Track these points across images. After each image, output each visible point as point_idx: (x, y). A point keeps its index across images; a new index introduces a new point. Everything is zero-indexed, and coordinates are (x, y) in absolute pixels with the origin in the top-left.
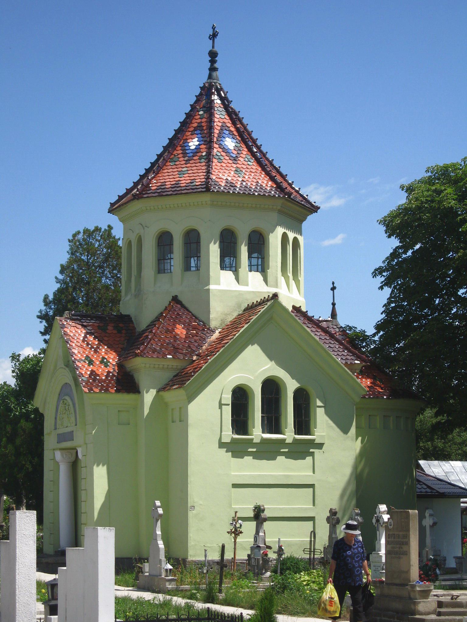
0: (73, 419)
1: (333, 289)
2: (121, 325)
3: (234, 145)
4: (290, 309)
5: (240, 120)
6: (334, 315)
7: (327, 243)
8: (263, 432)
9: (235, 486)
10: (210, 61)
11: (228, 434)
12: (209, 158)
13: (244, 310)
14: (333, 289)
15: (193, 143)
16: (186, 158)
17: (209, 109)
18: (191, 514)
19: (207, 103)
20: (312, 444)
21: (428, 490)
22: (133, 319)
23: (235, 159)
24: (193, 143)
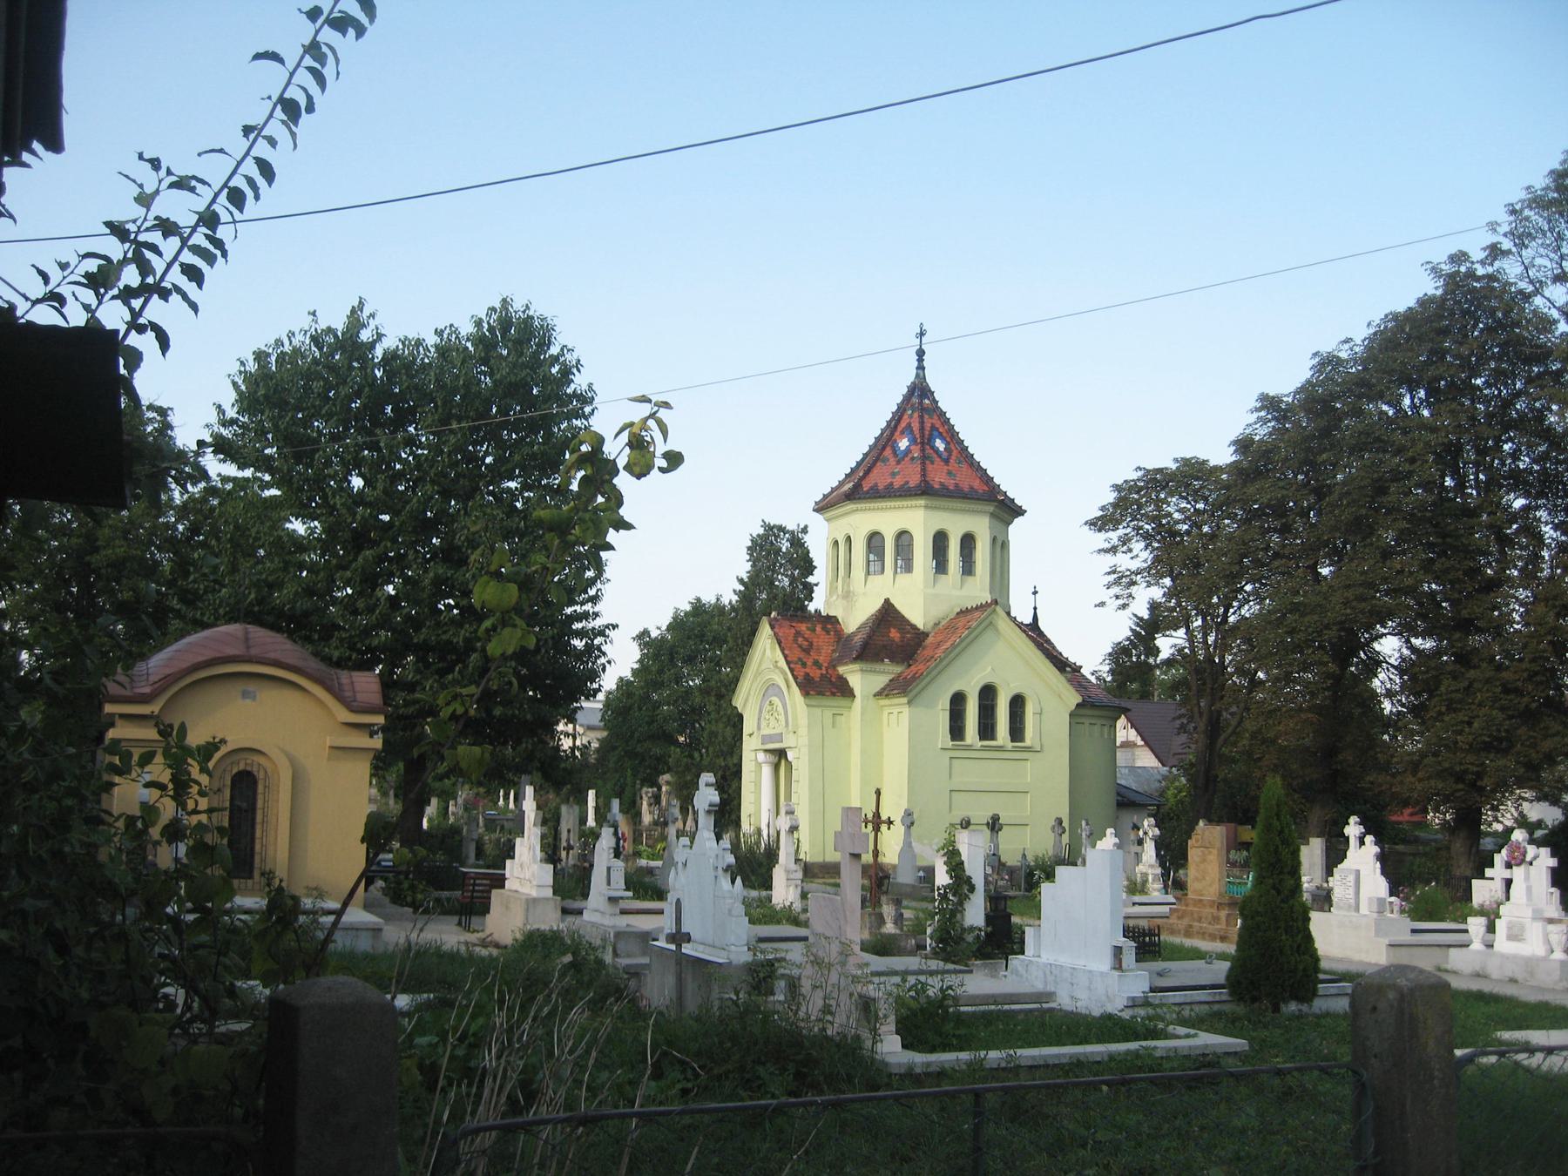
0: (782, 718)
1: (1035, 593)
2: (829, 626)
10: (918, 360)
14: (1035, 593)
22: (840, 620)
23: (947, 461)
24: (903, 444)
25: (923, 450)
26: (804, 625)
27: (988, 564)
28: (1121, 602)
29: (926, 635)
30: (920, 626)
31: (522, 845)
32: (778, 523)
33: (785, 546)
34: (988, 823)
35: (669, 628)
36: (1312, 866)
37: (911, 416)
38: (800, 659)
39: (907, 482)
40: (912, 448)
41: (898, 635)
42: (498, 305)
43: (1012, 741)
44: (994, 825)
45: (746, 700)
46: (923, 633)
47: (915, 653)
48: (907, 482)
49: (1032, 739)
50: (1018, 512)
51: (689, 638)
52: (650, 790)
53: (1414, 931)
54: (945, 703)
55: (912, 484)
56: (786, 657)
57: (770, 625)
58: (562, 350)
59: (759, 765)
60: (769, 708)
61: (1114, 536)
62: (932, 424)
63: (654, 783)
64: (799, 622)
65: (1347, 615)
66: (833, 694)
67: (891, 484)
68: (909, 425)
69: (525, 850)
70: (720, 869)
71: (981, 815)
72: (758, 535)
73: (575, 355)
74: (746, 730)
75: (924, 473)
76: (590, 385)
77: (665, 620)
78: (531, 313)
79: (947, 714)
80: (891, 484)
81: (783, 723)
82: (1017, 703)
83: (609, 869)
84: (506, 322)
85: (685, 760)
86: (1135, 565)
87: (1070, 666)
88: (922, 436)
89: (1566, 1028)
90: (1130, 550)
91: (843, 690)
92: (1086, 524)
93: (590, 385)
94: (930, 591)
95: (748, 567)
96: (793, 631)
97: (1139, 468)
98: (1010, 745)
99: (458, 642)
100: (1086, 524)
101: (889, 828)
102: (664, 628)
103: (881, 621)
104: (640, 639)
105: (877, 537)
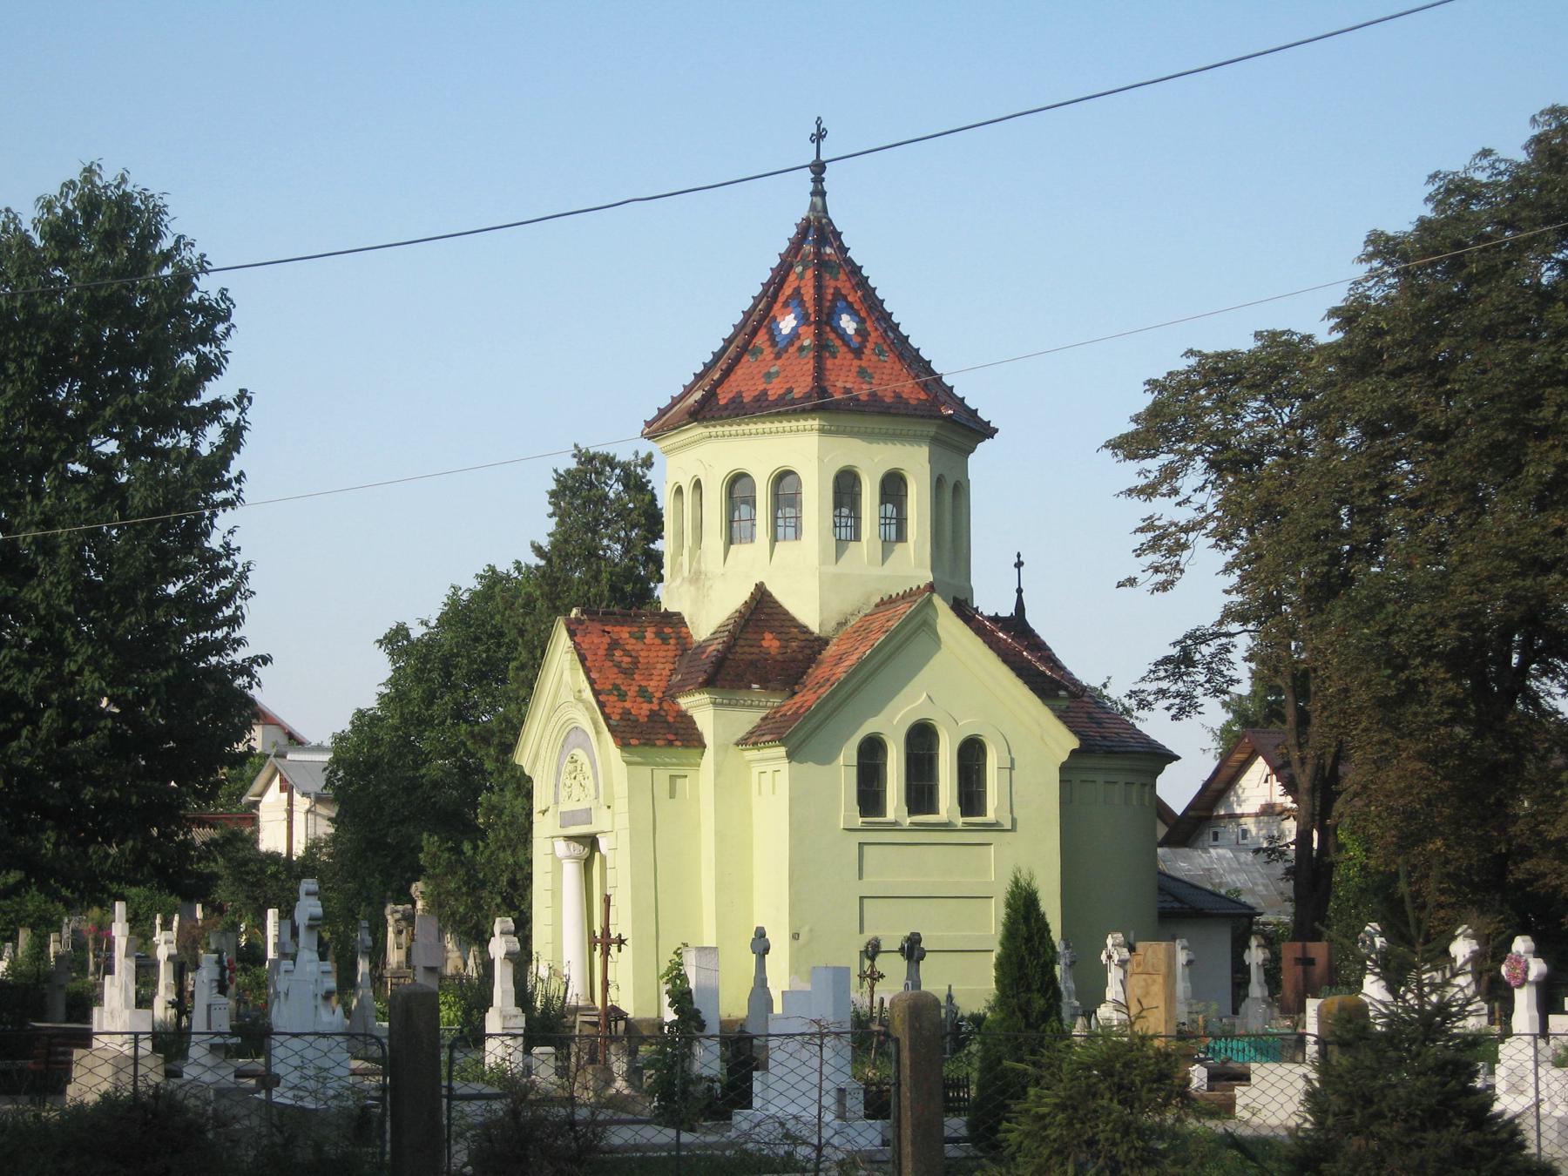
0: (590, 783)
1: (1019, 565)
2: (667, 630)
7: (1315, 845)
9: (861, 877)
10: (814, 180)
13: (877, 606)
14: (1019, 565)
19: (884, 336)
23: (858, 353)
25: (819, 336)
26: (626, 629)
27: (928, 523)
28: (1161, 577)
29: (823, 642)
30: (814, 627)
31: (112, 984)
32: (603, 450)
33: (614, 489)
34: (902, 950)
35: (444, 620)
37: (801, 277)
38: (616, 687)
39: (790, 390)
40: (802, 330)
41: (777, 643)
42: (77, 178)
43: (963, 814)
44: (913, 950)
45: (537, 755)
46: (818, 639)
47: (804, 673)
48: (790, 390)
49: (896, 810)
50: (987, 432)
51: (477, 639)
52: (400, 907)
54: (848, 755)
55: (798, 392)
56: (592, 682)
57: (569, 630)
58: (178, 242)
59: (557, 863)
60: (571, 767)
61: (1153, 465)
62: (836, 288)
63: (404, 896)
64: (617, 623)
65: (1472, 603)
66: (670, 743)
67: (764, 393)
69: (116, 991)
70: (319, 997)
71: (893, 938)
72: (568, 471)
73: (197, 252)
74: (538, 805)
75: (820, 372)
76: (223, 292)
77: (433, 609)
78: (129, 189)
79: (854, 771)
80: (764, 393)
81: (592, 791)
82: (972, 753)
83: (209, 1006)
84: (91, 203)
85: (446, 855)
86: (1185, 515)
87: (1066, 688)
88: (819, 312)
90: (1175, 491)
91: (686, 736)
92: (1106, 447)
93: (223, 292)
94: (832, 569)
95: (551, 524)
96: (607, 640)
97: (1190, 353)
98: (960, 821)
99: (24, 694)
100: (1106, 447)
101: (620, 950)
102: (433, 623)
103: (747, 621)
104: (390, 641)
105: (744, 481)
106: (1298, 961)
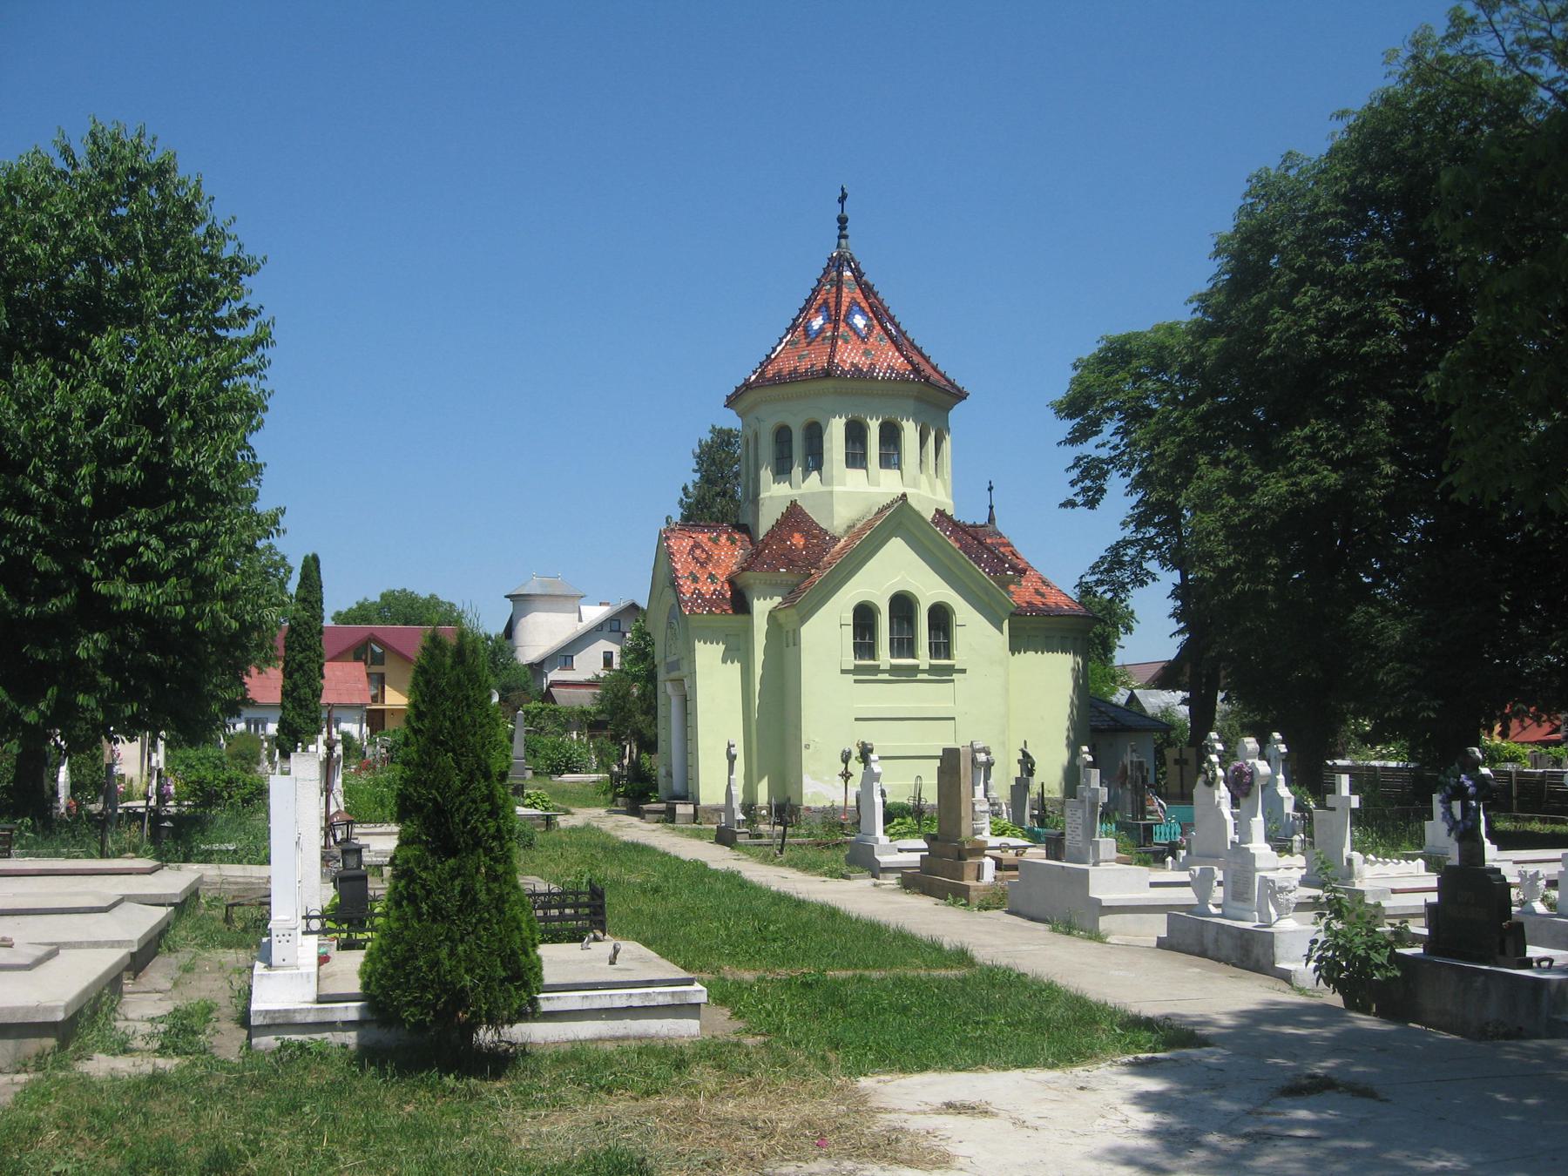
1: (990, 489)
3: (864, 322)
4: (929, 515)
5: (875, 295)
6: (991, 519)
8: (892, 656)
9: (856, 719)
11: (850, 661)
12: (834, 339)
14: (990, 489)
15: (817, 323)
16: (808, 340)
17: (839, 284)
18: (805, 753)
20: (950, 670)
21: (1112, 723)
24: (817, 323)
36: (965, 769)
50: (960, 395)
53: (1153, 885)
68: (826, 302)
89: (2, 1009)
106: (1176, 762)
